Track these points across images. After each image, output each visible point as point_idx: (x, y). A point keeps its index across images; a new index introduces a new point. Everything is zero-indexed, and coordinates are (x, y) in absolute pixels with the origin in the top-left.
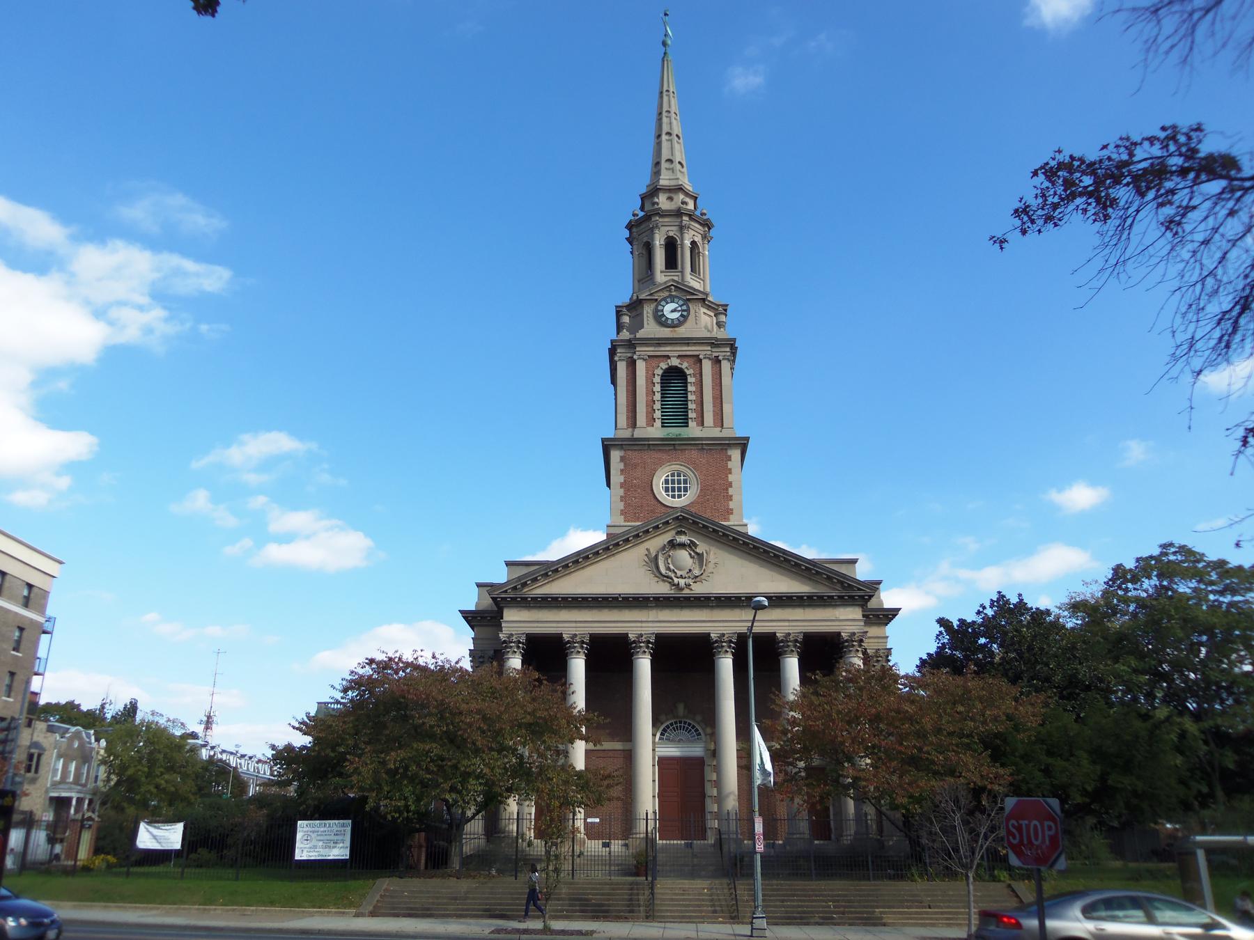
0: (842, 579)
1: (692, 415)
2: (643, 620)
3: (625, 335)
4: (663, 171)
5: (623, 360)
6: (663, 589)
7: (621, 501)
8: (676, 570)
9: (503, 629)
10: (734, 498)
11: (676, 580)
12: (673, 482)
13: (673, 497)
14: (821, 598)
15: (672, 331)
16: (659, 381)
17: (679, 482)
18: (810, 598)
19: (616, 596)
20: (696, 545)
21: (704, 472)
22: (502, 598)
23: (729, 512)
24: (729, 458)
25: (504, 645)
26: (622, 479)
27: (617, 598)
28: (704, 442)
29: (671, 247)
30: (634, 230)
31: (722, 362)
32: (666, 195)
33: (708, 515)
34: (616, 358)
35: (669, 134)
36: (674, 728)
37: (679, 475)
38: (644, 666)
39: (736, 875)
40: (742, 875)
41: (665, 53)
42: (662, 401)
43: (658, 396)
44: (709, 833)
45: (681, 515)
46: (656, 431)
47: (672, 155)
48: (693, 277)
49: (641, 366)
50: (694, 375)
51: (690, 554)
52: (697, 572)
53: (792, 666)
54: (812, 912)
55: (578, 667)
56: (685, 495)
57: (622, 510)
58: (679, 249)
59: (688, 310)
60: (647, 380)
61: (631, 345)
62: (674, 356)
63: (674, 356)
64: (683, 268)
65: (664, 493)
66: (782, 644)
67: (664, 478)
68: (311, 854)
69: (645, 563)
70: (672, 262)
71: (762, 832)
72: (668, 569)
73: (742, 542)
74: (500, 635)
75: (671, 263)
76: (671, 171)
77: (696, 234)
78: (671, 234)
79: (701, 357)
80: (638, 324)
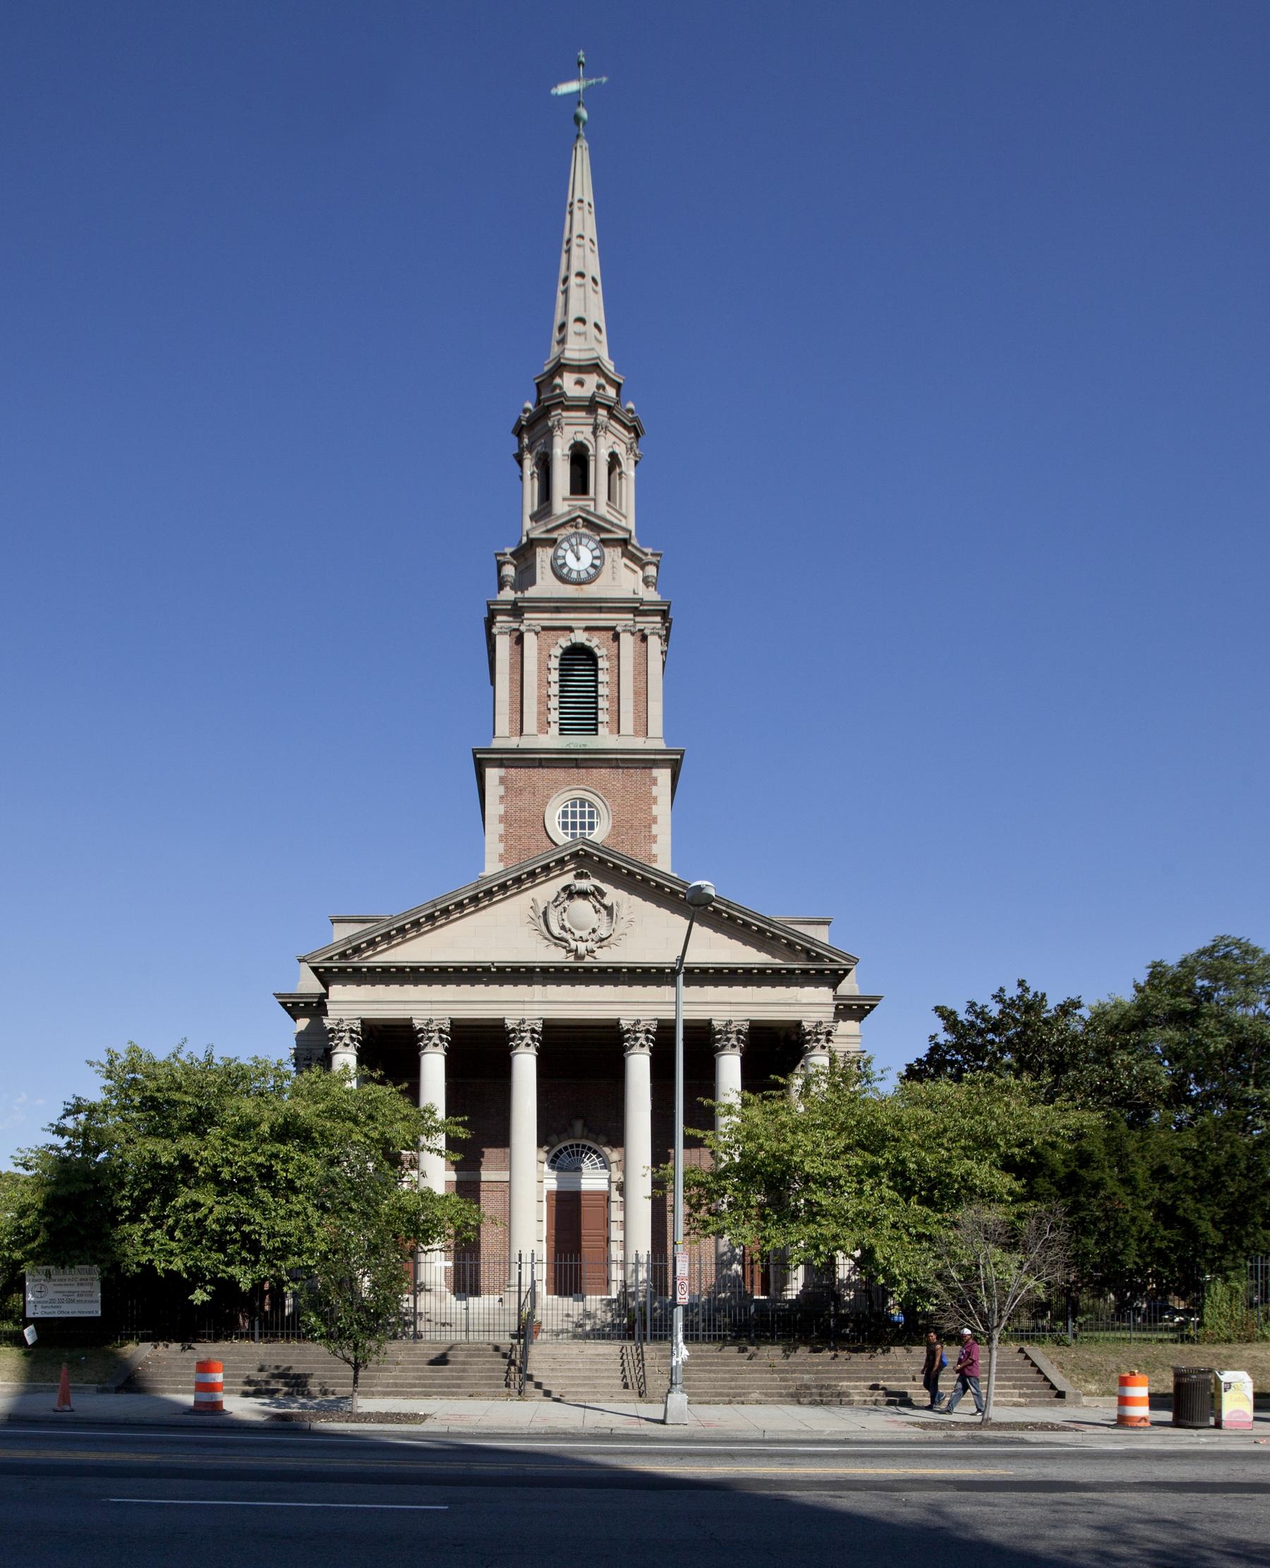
0: (809, 946)
1: (602, 716)
2: (527, 999)
3: (508, 594)
4: (571, 338)
5: (506, 633)
6: (556, 956)
7: (501, 841)
8: (573, 930)
9: (329, 1013)
10: (659, 838)
12: (574, 815)
14: (777, 971)
16: (557, 666)
17: (582, 815)
18: (762, 971)
20: (603, 894)
21: (619, 801)
22: (325, 968)
24: (654, 782)
25: (330, 1035)
26: (501, 810)
27: (489, 968)
29: (579, 458)
31: (649, 638)
32: (575, 376)
33: (624, 850)
34: (495, 630)
35: (581, 201)
36: (568, 1154)
37: (582, 806)
38: (525, 1066)
39: (645, 1339)
40: (654, 1338)
42: (561, 670)
43: (555, 689)
44: (614, 1285)
45: (582, 849)
46: (552, 740)
48: (611, 511)
49: (530, 640)
50: (608, 658)
51: (594, 907)
52: (603, 932)
53: (730, 1068)
54: (749, 1387)
55: (433, 1066)
57: (501, 855)
59: (601, 558)
61: (516, 611)
63: (579, 628)
66: (719, 1036)
67: (561, 809)
68: (47, 1310)
70: (580, 485)
71: (686, 1275)
72: (563, 928)
74: (325, 1021)
75: (580, 485)
77: (617, 441)
78: (580, 438)
79: (619, 629)
80: (526, 577)
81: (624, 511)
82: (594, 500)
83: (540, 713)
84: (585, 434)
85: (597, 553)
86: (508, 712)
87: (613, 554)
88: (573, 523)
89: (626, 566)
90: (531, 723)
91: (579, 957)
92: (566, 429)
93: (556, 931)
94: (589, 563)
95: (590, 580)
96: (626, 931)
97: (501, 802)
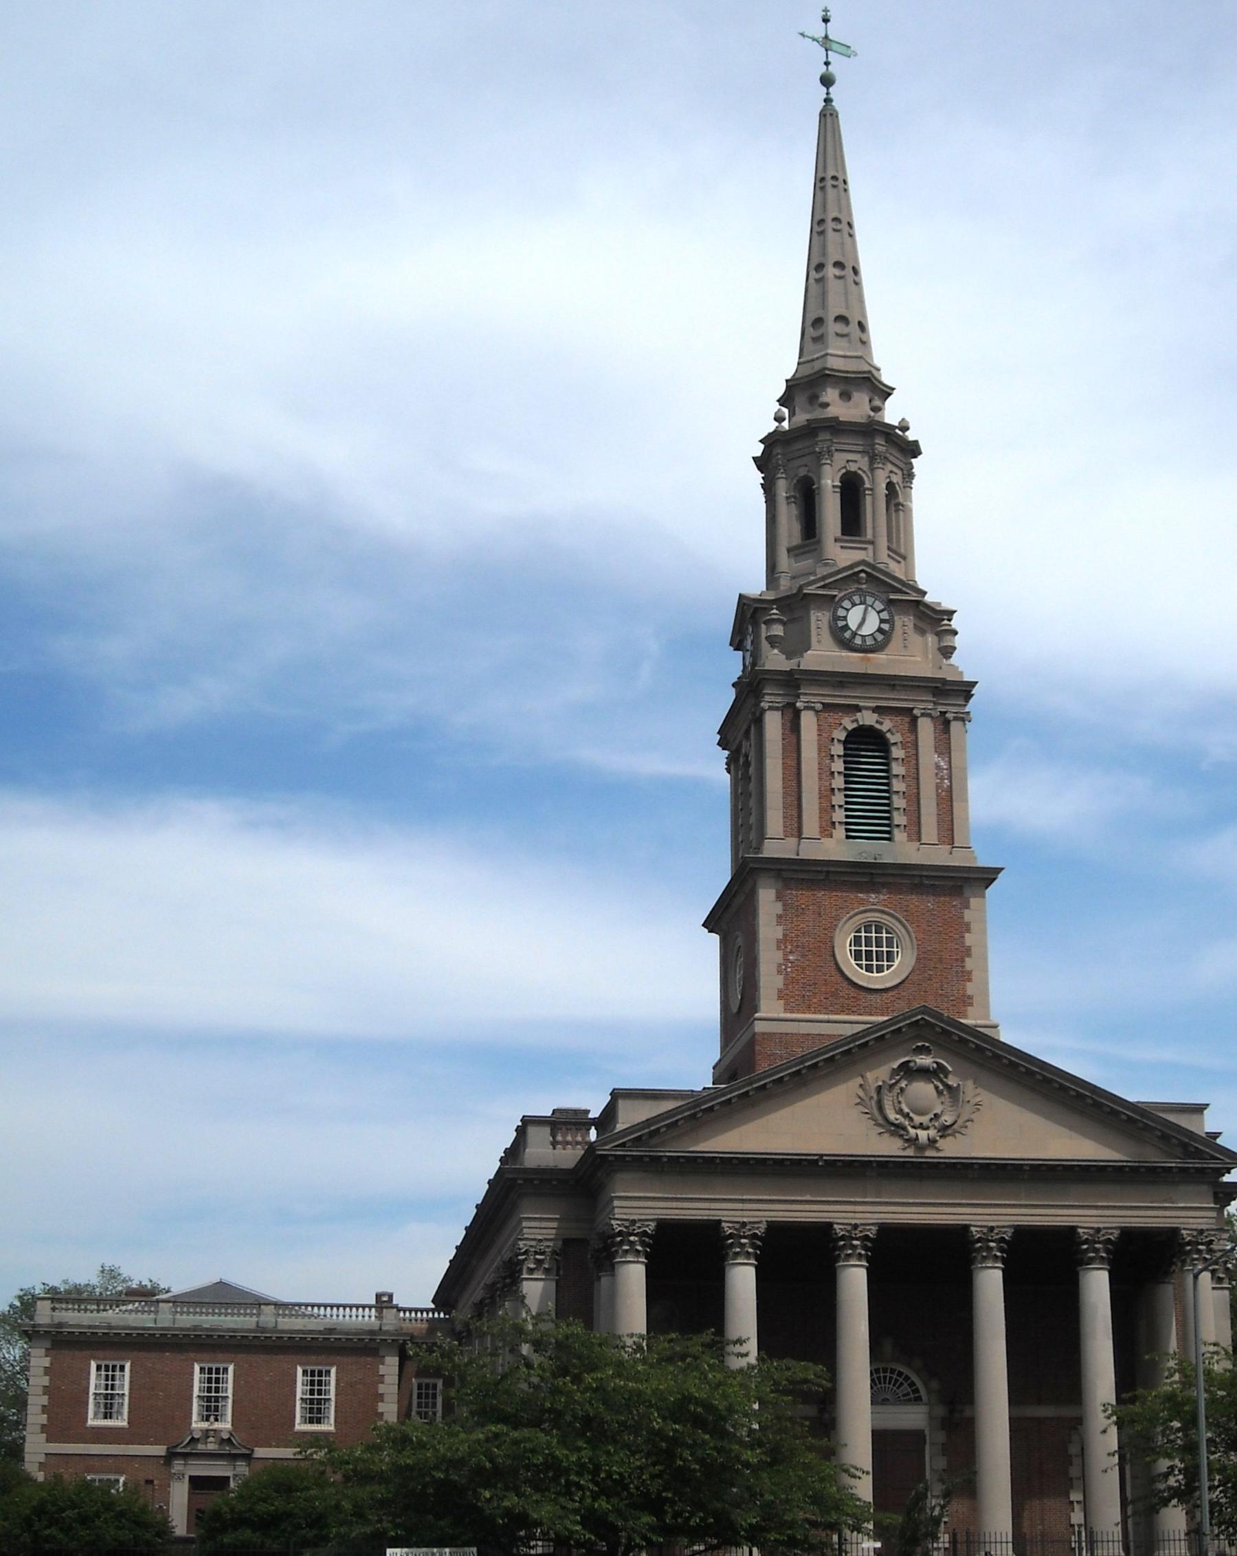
1: (899, 818)
6: (890, 1147)
11: (912, 1131)
13: (869, 969)
15: (862, 659)
19: (816, 1158)
23: (967, 1001)
26: (779, 933)
28: (924, 873)
29: (851, 489)
30: (778, 450)
47: (847, 308)
48: (890, 553)
49: (808, 721)
50: (904, 745)
51: (936, 1088)
52: (947, 1119)
56: (889, 967)
60: (820, 750)
62: (867, 708)
63: (867, 708)
65: (853, 962)
69: (859, 1100)
70: (852, 524)
73: (1126, 1118)
75: (852, 524)
76: (845, 339)
77: (895, 469)
78: (853, 467)
80: (797, 644)
81: (902, 551)
83: (822, 810)
84: (859, 464)
85: (885, 615)
86: (781, 805)
87: (905, 622)
88: (855, 578)
89: (842, 547)
90: (811, 824)
91: (921, 1148)
92: (837, 455)
93: (892, 1116)
94: (876, 627)
95: (878, 648)
96: (973, 1116)
97: (779, 923)
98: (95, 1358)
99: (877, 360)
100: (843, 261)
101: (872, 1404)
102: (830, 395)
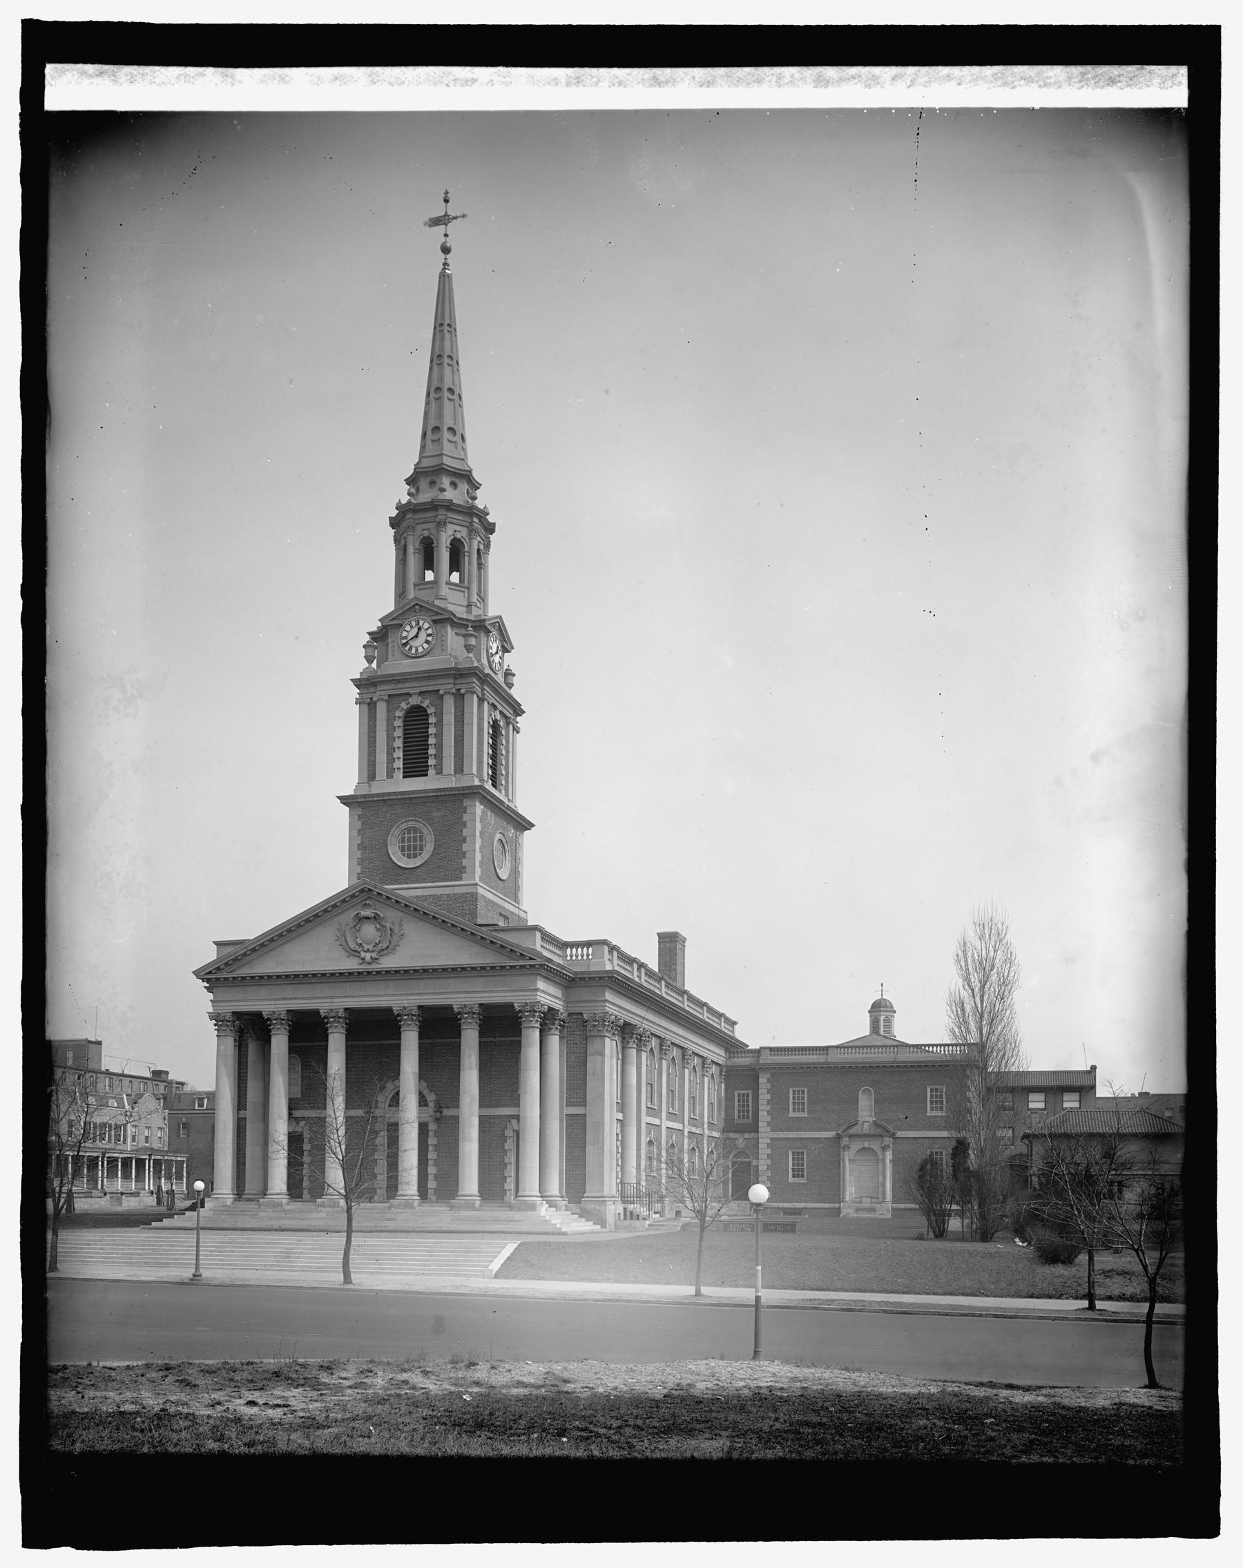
6: (351, 964)
14: (502, 967)
41: (445, 264)
58: (466, 558)
63: (414, 694)
64: (469, 582)
65: (400, 853)
76: (453, 445)
78: (458, 536)
82: (468, 588)
84: (462, 533)
98: (929, 1085)
99: (470, 464)
100: (453, 387)
101: (480, 1107)
102: (446, 481)
